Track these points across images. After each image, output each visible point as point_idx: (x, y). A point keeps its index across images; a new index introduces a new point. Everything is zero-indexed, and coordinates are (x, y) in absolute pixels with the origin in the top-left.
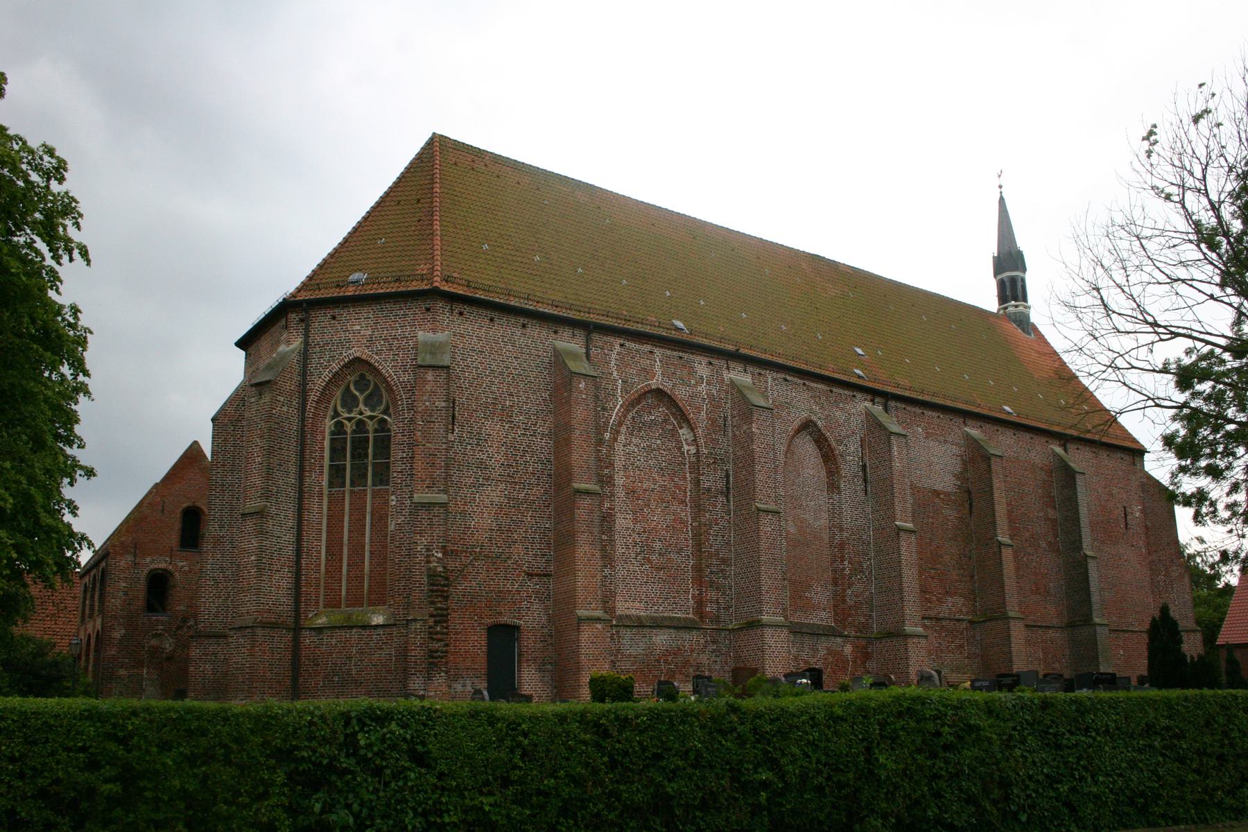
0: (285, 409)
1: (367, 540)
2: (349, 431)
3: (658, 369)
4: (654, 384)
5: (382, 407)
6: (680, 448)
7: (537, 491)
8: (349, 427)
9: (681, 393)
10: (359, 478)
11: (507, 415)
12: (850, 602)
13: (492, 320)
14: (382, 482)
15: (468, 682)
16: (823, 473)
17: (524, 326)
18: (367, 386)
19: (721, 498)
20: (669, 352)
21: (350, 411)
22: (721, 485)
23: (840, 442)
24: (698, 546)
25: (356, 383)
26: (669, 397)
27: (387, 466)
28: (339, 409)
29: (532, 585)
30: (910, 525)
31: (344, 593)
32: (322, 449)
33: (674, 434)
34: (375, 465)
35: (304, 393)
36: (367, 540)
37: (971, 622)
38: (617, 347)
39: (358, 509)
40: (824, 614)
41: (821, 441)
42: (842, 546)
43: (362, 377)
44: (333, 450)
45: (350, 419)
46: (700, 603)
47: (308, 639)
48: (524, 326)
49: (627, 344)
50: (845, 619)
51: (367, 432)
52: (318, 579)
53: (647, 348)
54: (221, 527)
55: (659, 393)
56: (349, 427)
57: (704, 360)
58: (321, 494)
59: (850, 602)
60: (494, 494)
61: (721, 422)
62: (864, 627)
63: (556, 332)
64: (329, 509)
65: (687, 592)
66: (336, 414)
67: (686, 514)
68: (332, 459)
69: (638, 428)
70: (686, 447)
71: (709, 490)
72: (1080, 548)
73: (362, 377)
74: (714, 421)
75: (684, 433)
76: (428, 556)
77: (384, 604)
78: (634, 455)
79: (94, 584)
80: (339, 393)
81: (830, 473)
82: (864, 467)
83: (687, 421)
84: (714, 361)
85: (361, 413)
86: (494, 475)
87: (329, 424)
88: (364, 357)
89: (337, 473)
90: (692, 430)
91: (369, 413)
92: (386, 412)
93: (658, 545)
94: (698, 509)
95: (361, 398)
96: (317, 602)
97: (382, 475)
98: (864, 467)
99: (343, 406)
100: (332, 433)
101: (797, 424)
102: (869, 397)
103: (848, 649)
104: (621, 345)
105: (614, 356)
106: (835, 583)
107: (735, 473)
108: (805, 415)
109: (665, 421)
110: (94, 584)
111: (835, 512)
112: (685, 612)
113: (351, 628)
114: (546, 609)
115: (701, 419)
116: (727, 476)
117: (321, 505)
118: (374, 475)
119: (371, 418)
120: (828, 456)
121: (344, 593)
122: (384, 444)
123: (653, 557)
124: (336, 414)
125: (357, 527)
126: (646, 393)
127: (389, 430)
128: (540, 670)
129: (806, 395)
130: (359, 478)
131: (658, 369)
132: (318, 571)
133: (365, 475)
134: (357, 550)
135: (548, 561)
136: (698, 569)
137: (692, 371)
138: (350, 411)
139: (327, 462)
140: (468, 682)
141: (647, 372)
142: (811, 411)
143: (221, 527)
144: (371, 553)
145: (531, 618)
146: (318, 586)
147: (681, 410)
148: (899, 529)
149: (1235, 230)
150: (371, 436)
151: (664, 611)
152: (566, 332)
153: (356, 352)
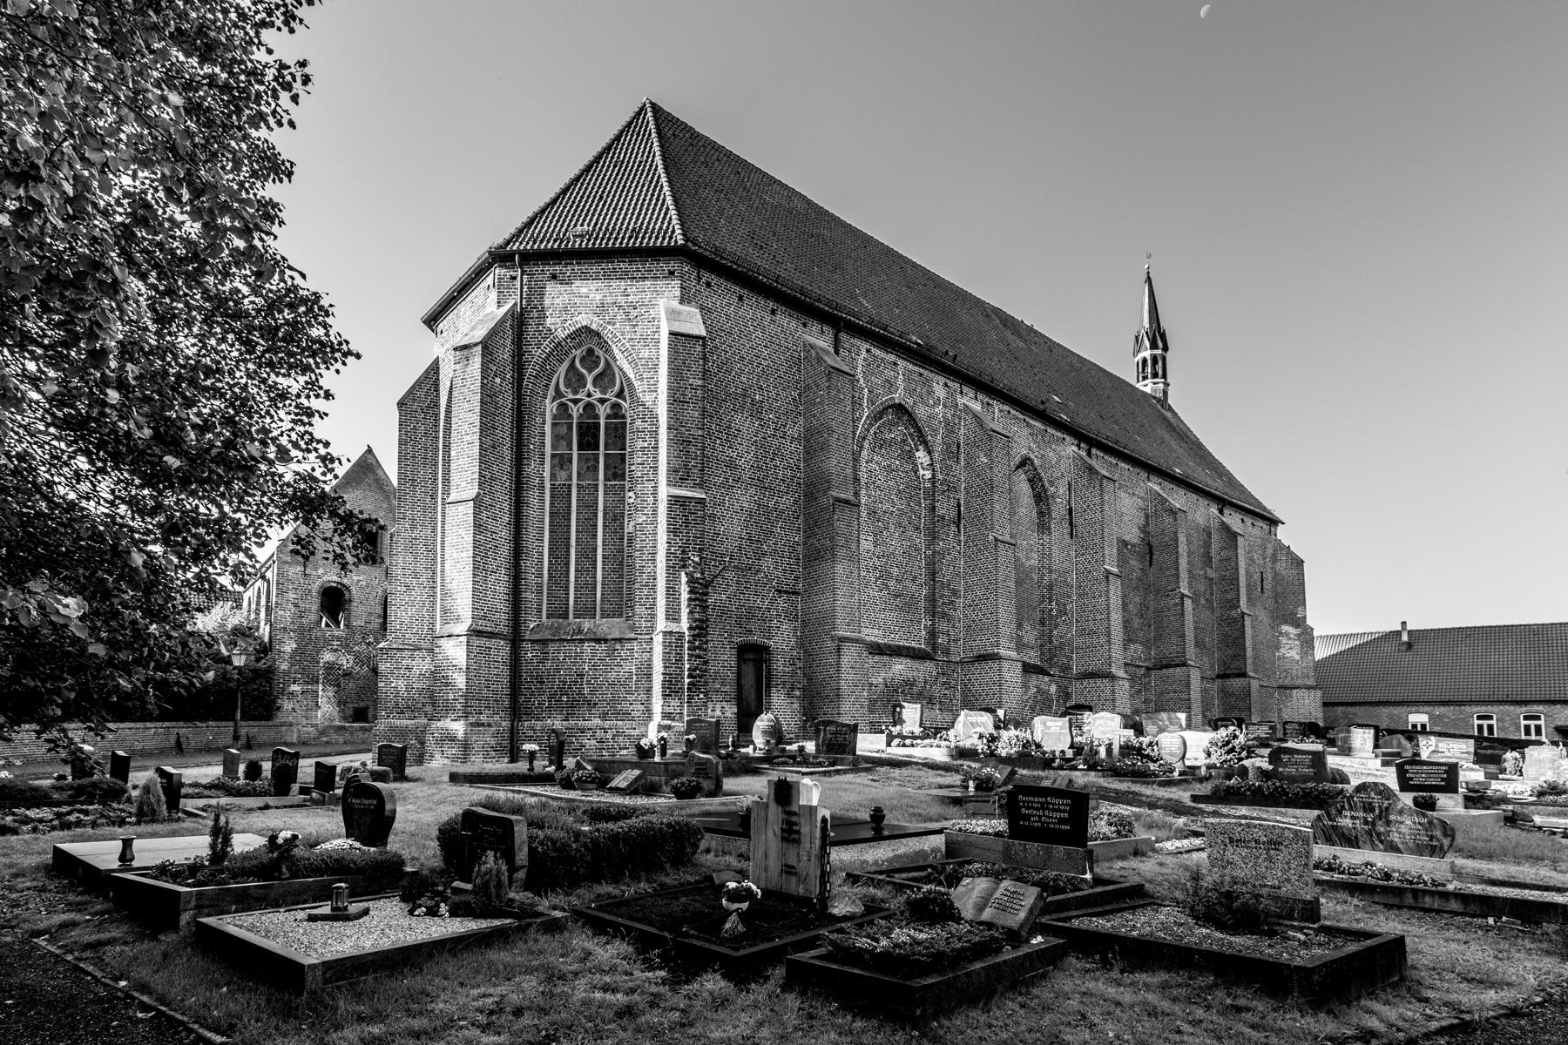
0: (498, 380)
1: (600, 542)
2: (575, 415)
3: (900, 383)
4: (898, 397)
5: (617, 388)
6: (916, 472)
7: (786, 501)
8: (576, 411)
9: (921, 412)
10: (589, 468)
11: (756, 411)
12: (1056, 643)
13: (740, 298)
14: (615, 477)
15: (718, 707)
16: (1034, 514)
17: (773, 312)
18: (597, 364)
19: (953, 528)
20: (911, 367)
21: (575, 392)
22: (953, 514)
23: (1052, 483)
24: (933, 575)
25: (582, 360)
26: (910, 415)
27: (623, 458)
28: (562, 388)
29: (782, 603)
30: (1115, 570)
31: (571, 602)
32: (543, 434)
33: (910, 456)
34: (606, 455)
35: (519, 366)
36: (600, 542)
37: (1148, 669)
38: (864, 354)
39: (588, 506)
40: (1032, 653)
41: (1035, 480)
42: (1050, 587)
43: (590, 352)
44: (557, 438)
45: (576, 402)
46: (933, 634)
47: (529, 653)
48: (773, 312)
49: (874, 350)
50: (1051, 659)
51: (597, 417)
52: (541, 585)
53: (892, 358)
54: (413, 527)
55: (900, 409)
56: (576, 411)
57: (942, 380)
58: (541, 487)
59: (1056, 643)
60: (744, 499)
61: (954, 448)
62: (1066, 668)
63: (805, 325)
64: (552, 505)
65: (919, 622)
66: (558, 394)
67: (920, 540)
68: (554, 447)
69: (880, 444)
70: (921, 472)
71: (943, 518)
72: (1237, 606)
73: (590, 352)
74: (949, 446)
75: (922, 456)
76: (683, 560)
77: (620, 616)
78: (876, 475)
79: (259, 597)
80: (562, 369)
81: (1041, 514)
82: (1070, 510)
83: (925, 443)
84: (950, 384)
85: (589, 395)
86: (745, 477)
87: (550, 407)
88: (594, 327)
89: (562, 462)
90: (930, 453)
91: (599, 395)
92: (620, 395)
93: (895, 571)
94: (933, 537)
95: (590, 379)
96: (540, 611)
97: (617, 470)
98: (1070, 510)
99: (567, 386)
100: (555, 417)
101: (1018, 460)
102: (841, 521)
103: (1053, 688)
104: (868, 351)
105: (860, 362)
106: (1042, 623)
107: (967, 503)
108: (1024, 452)
109: (904, 441)
110: (259, 597)
111: (1045, 555)
112: (919, 642)
113: (582, 641)
114: (795, 629)
115: (937, 442)
116: (959, 505)
117: (542, 500)
118: (607, 467)
119: (602, 401)
120: (1041, 497)
121: (571, 602)
122: (618, 432)
123: (892, 584)
124: (558, 394)
125: (588, 527)
126: (886, 409)
127: (623, 417)
128: (789, 695)
129: (1026, 431)
130: (589, 468)
131: (900, 383)
132: (541, 576)
133: (596, 469)
134: (587, 554)
135: (797, 578)
136: (932, 600)
137: (931, 392)
138: (575, 392)
139: (548, 450)
140: (718, 707)
141: (890, 385)
142: (1030, 449)
143: (413, 527)
144: (604, 557)
145: (782, 640)
146: (540, 592)
147: (920, 431)
148: (1108, 573)
149: (731, 545)
150: (602, 422)
151: (898, 640)
152: (815, 327)
153: (583, 320)
